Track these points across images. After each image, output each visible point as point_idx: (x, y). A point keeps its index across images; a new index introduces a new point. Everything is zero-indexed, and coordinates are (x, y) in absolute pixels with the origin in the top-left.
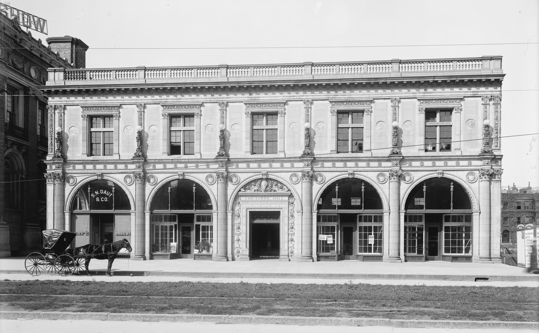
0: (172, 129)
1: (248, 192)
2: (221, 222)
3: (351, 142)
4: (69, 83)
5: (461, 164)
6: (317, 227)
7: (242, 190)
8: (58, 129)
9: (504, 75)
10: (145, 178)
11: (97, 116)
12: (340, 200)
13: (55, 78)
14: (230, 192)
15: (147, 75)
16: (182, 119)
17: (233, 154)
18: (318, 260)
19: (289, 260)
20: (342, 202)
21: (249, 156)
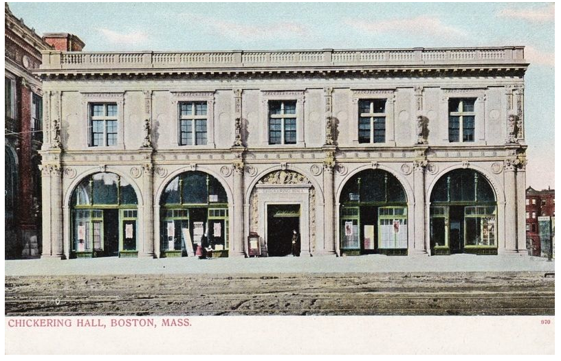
0: (94, 118)
1: (266, 184)
2: (238, 216)
3: (193, 132)
4: (66, 66)
5: (474, 155)
6: (340, 220)
7: (260, 182)
8: (54, 117)
9: (527, 65)
10: (62, 172)
11: (100, 104)
12: (216, 196)
13: (50, 62)
14: (247, 184)
15: (154, 60)
16: (104, 107)
17: (251, 144)
18: (161, 257)
19: (311, 256)
20: (219, 198)
21: (447, 144)
